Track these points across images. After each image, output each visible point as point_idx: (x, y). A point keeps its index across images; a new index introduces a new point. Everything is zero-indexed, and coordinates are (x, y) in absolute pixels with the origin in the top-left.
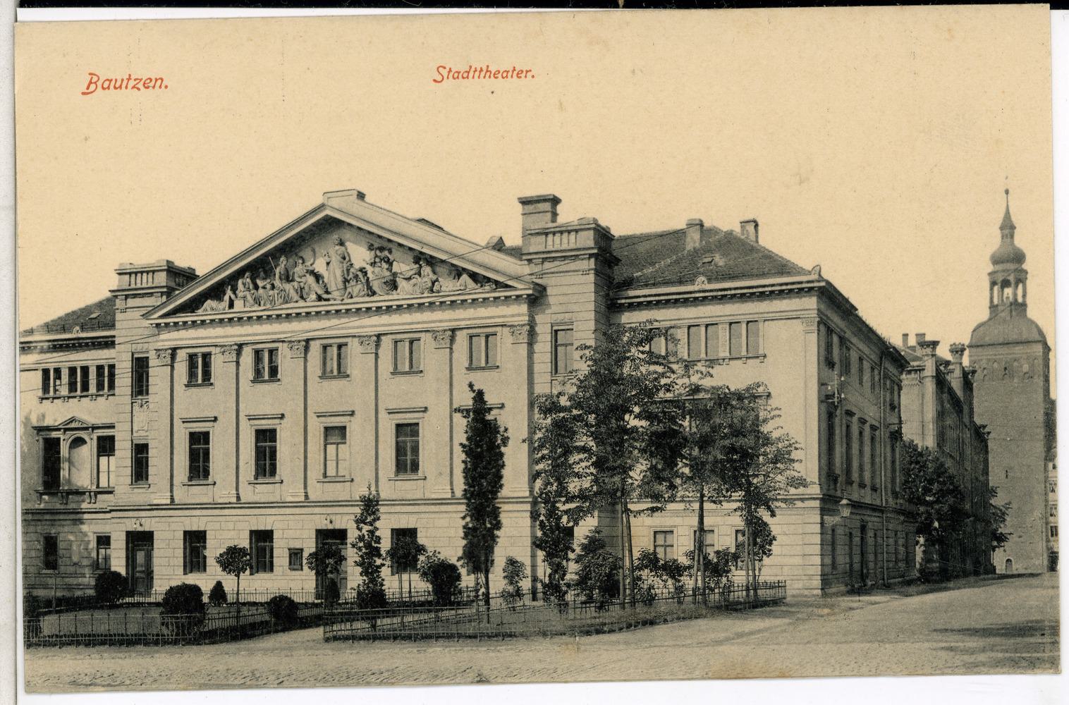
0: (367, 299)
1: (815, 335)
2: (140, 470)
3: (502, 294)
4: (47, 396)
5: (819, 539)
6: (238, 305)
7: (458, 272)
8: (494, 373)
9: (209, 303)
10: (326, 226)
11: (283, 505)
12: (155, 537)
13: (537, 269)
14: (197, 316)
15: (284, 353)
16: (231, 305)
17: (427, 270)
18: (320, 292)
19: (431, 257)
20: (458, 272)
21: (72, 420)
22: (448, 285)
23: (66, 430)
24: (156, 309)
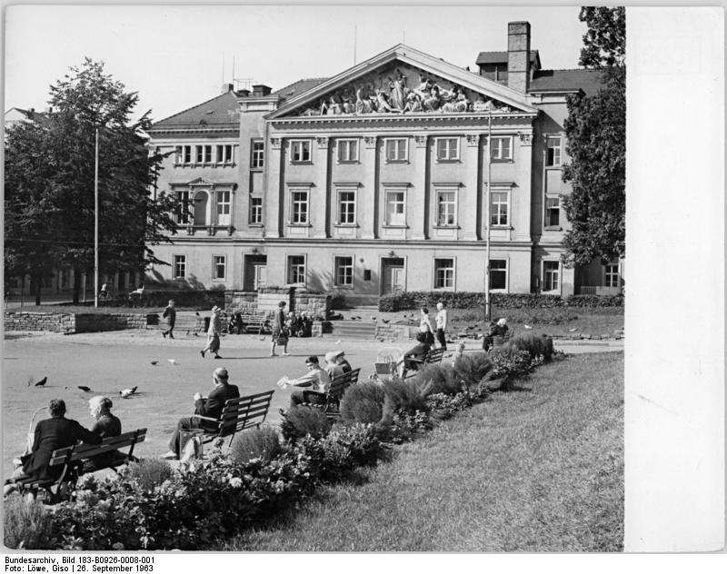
0: (423, 113)
1: (530, 148)
2: (255, 216)
3: (516, 114)
4: (200, 163)
5: (419, 289)
6: (330, 112)
7: (485, 99)
8: (509, 165)
9: (309, 111)
10: (392, 67)
11: (457, 243)
12: (268, 259)
13: (538, 100)
14: (301, 119)
15: (313, 146)
16: (325, 112)
17: (461, 96)
18: (388, 107)
19: (466, 88)
20: (485, 99)
21: (200, 180)
22: (479, 106)
23: (193, 187)
24: (273, 113)
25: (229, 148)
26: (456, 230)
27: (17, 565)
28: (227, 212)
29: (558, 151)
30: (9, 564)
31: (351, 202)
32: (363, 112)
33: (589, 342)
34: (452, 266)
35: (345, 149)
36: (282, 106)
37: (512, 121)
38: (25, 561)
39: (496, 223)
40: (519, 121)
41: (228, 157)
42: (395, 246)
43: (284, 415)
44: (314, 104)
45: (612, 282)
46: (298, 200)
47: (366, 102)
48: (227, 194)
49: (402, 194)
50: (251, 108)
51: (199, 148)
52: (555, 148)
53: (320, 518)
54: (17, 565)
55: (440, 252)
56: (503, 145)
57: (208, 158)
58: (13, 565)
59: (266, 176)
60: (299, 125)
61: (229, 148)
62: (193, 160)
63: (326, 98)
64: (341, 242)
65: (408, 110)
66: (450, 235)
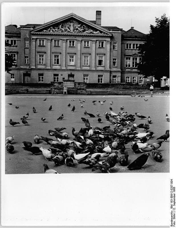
6: (51, 31)
9: (45, 31)
16: (50, 31)
25: (15, 41)
26: (103, 67)
27: (173, 223)
28: (73, 61)
29: (116, 46)
30: (173, 225)
31: (43, 58)
32: (62, 32)
33: (158, 94)
34: (43, 76)
35: (41, 42)
36: (35, 29)
37: (105, 37)
38: (172, 220)
39: (41, 63)
40: (107, 37)
41: (15, 43)
42: (72, 71)
43: (74, 134)
44: (46, 29)
45: (56, 80)
46: (56, 57)
47: (63, 29)
48: (15, 55)
49: (59, 56)
50: (24, 29)
51: (134, 45)
52: (115, 45)
53: (146, 169)
54: (173, 223)
55: (55, 72)
56: (42, 42)
57: (130, 47)
58: (173, 224)
59: (30, 50)
60: (42, 35)
61: (15, 41)
62: (132, 48)
63: (49, 27)
64: (55, 70)
65: (75, 32)
66: (58, 67)
